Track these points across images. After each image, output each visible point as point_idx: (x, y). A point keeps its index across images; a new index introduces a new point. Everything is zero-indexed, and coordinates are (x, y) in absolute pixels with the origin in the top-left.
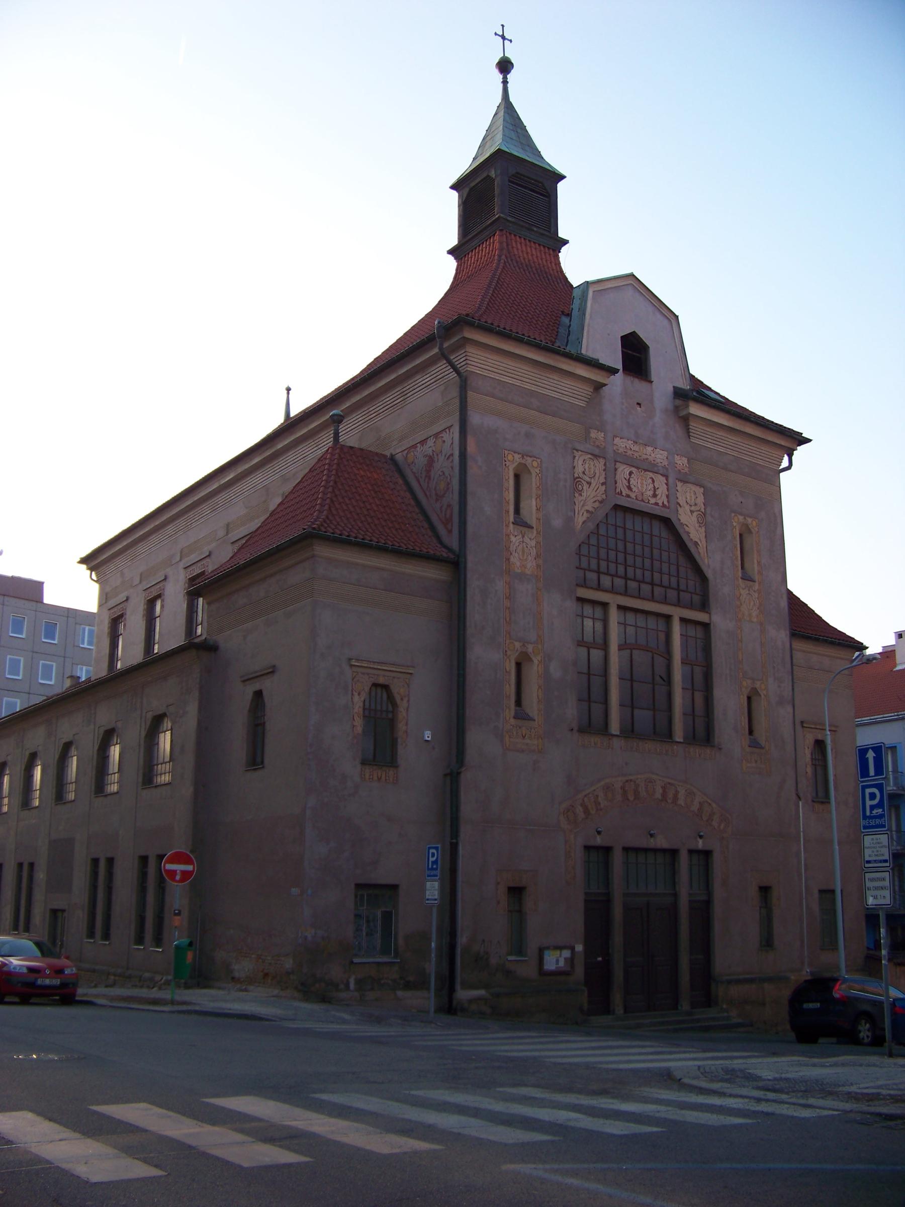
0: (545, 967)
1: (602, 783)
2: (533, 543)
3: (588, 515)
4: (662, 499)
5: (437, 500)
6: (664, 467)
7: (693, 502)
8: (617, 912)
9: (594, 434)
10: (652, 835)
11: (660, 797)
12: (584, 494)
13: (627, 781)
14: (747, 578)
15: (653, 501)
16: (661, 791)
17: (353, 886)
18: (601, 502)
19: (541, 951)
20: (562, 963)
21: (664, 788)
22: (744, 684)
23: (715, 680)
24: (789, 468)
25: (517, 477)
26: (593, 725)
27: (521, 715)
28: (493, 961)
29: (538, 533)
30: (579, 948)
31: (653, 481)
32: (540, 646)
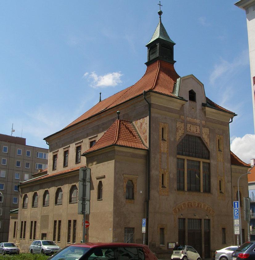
0: (169, 247)
2: (166, 145)
4: (198, 132)
5: (143, 134)
6: (199, 124)
8: (186, 234)
9: (182, 117)
10: (195, 216)
12: (179, 132)
14: (220, 150)
17: (124, 228)
21: (198, 204)
25: (163, 129)
26: (180, 188)
27: (163, 187)
28: (157, 246)
29: (168, 142)
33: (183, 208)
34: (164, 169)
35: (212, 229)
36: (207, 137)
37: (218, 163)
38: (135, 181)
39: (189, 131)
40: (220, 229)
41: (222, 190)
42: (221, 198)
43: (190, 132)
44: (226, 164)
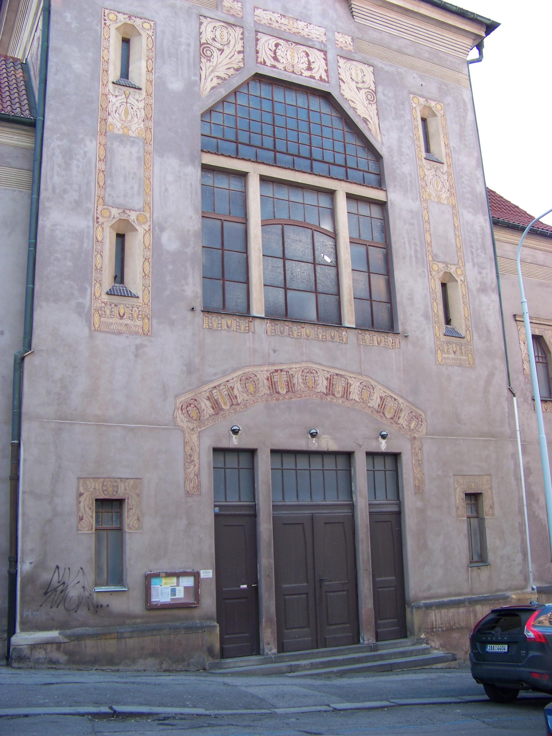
1: (240, 373)
2: (142, 105)
3: (220, 81)
7: (359, 79)
8: (265, 528)
10: (313, 435)
11: (325, 391)
12: (214, 60)
13: (276, 371)
15: (308, 73)
16: (325, 383)
18: (237, 70)
19: (148, 578)
20: (180, 594)
22: (435, 268)
23: (395, 260)
24: (479, 60)
28: (73, 593)
30: (207, 574)
31: (307, 55)
32: (148, 215)
36: (364, 97)
37: (426, 211)
39: (268, 63)
40: (458, 498)
41: (454, 322)
42: (452, 356)
44: (467, 216)
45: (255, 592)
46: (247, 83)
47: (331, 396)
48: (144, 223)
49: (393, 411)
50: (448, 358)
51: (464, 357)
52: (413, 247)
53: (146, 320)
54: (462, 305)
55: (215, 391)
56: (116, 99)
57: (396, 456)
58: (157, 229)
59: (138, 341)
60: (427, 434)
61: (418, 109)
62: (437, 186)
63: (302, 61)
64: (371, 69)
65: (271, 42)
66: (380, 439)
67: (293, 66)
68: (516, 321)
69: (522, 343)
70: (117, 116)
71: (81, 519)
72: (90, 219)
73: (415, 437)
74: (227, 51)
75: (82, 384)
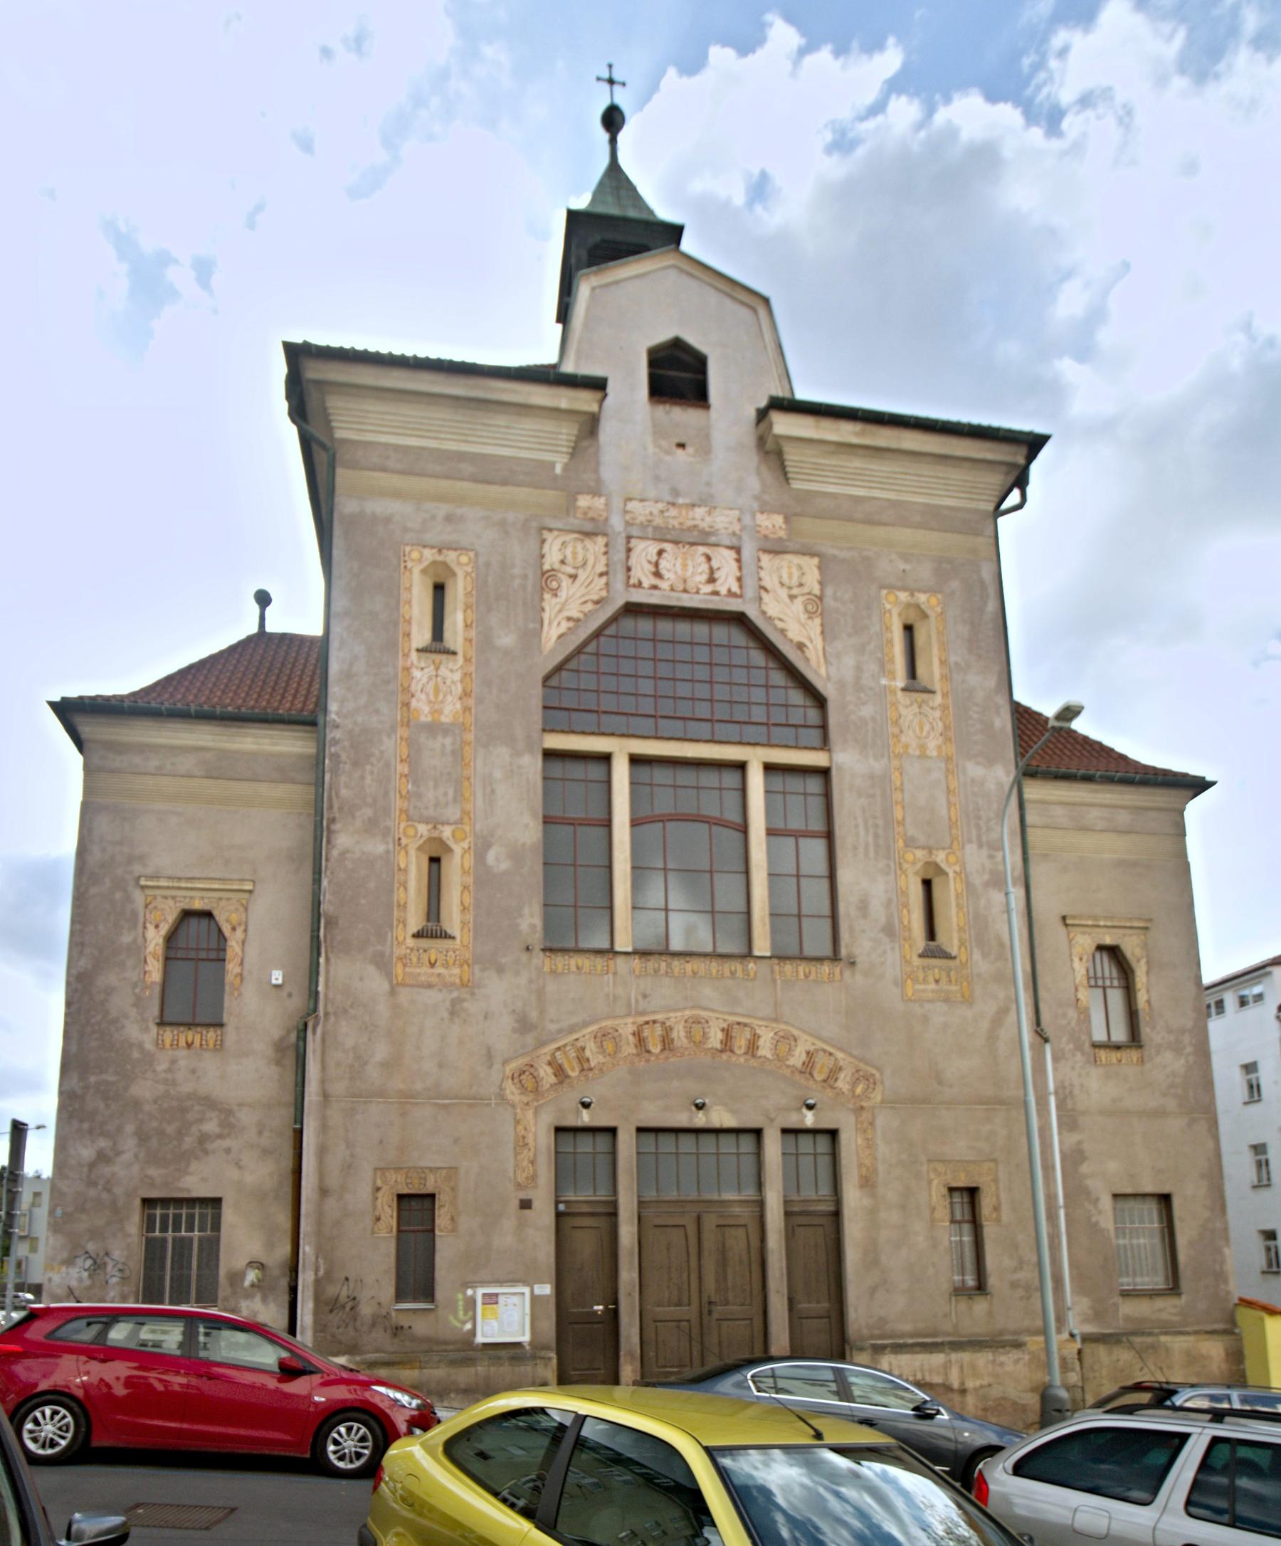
1: (594, 1028)
2: (457, 676)
3: (571, 624)
9: (583, 501)
10: (700, 1107)
11: (719, 1046)
12: (563, 594)
13: (647, 1023)
15: (709, 588)
16: (720, 1035)
18: (597, 602)
21: (727, 1032)
28: (366, 1310)
31: (709, 558)
32: (467, 829)
33: (595, 1059)
34: (436, 823)
35: (852, 1197)
36: (801, 608)
37: (906, 765)
38: (234, 917)
39: (646, 584)
42: (932, 986)
43: (655, 587)
44: (974, 770)
45: (613, 1315)
46: (614, 619)
47: (728, 1053)
48: (464, 840)
49: (826, 1070)
50: (923, 991)
51: (953, 988)
52: (871, 831)
53: (466, 967)
54: (954, 910)
55: (558, 1054)
56: (422, 673)
57: (833, 1134)
58: (481, 847)
59: (455, 994)
60: (882, 1102)
61: (895, 612)
62: (921, 728)
63: (700, 570)
64: (816, 561)
65: (650, 549)
66: (804, 1110)
67: (685, 581)
68: (1066, 925)
69: (1076, 960)
70: (423, 696)
71: (378, 1219)
72: (390, 840)
73: (862, 1108)
74: (582, 575)
75: (381, 1051)
